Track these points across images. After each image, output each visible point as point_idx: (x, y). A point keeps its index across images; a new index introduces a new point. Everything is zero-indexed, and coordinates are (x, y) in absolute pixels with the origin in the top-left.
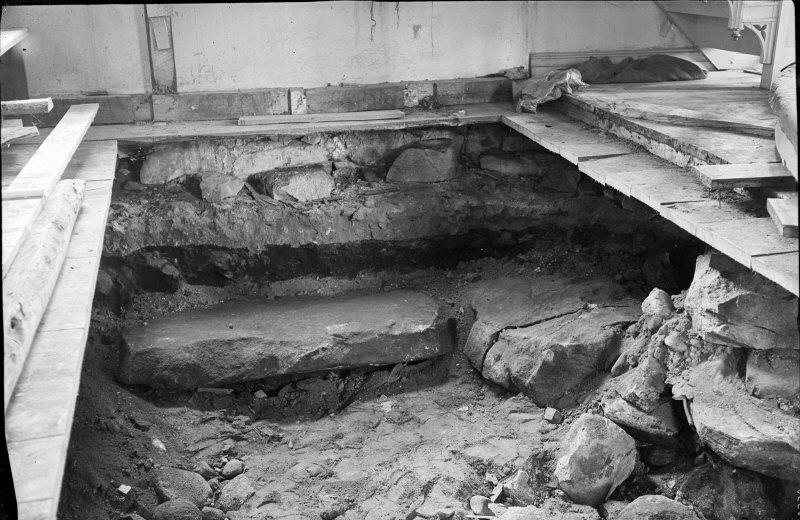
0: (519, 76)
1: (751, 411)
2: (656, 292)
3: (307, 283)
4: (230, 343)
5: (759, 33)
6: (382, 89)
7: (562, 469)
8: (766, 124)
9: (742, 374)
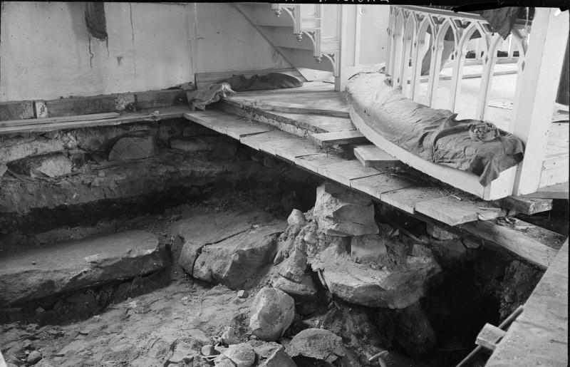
0: (189, 88)
1: (355, 270)
2: (295, 212)
3: (60, 233)
4: (17, 275)
5: (331, 59)
6: (100, 99)
7: (254, 323)
8: (344, 110)
9: (349, 252)
